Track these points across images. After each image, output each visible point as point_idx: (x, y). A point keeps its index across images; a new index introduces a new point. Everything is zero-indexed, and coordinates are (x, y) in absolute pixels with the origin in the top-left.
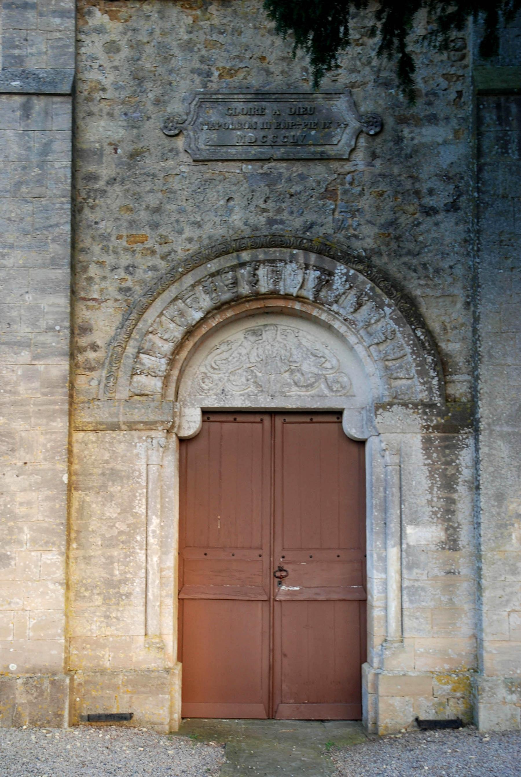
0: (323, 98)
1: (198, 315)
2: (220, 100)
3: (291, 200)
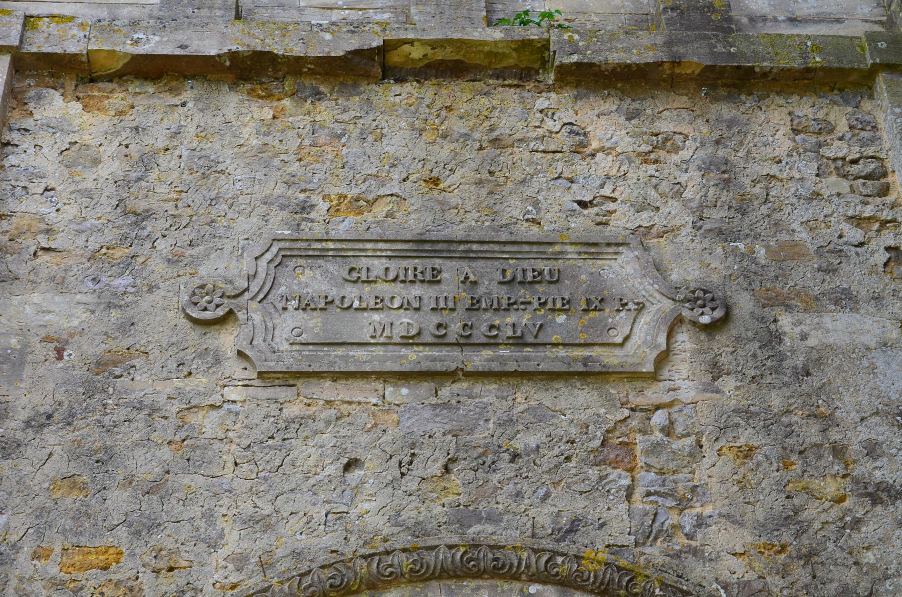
0: (580, 253)
2: (331, 253)
3: (516, 466)
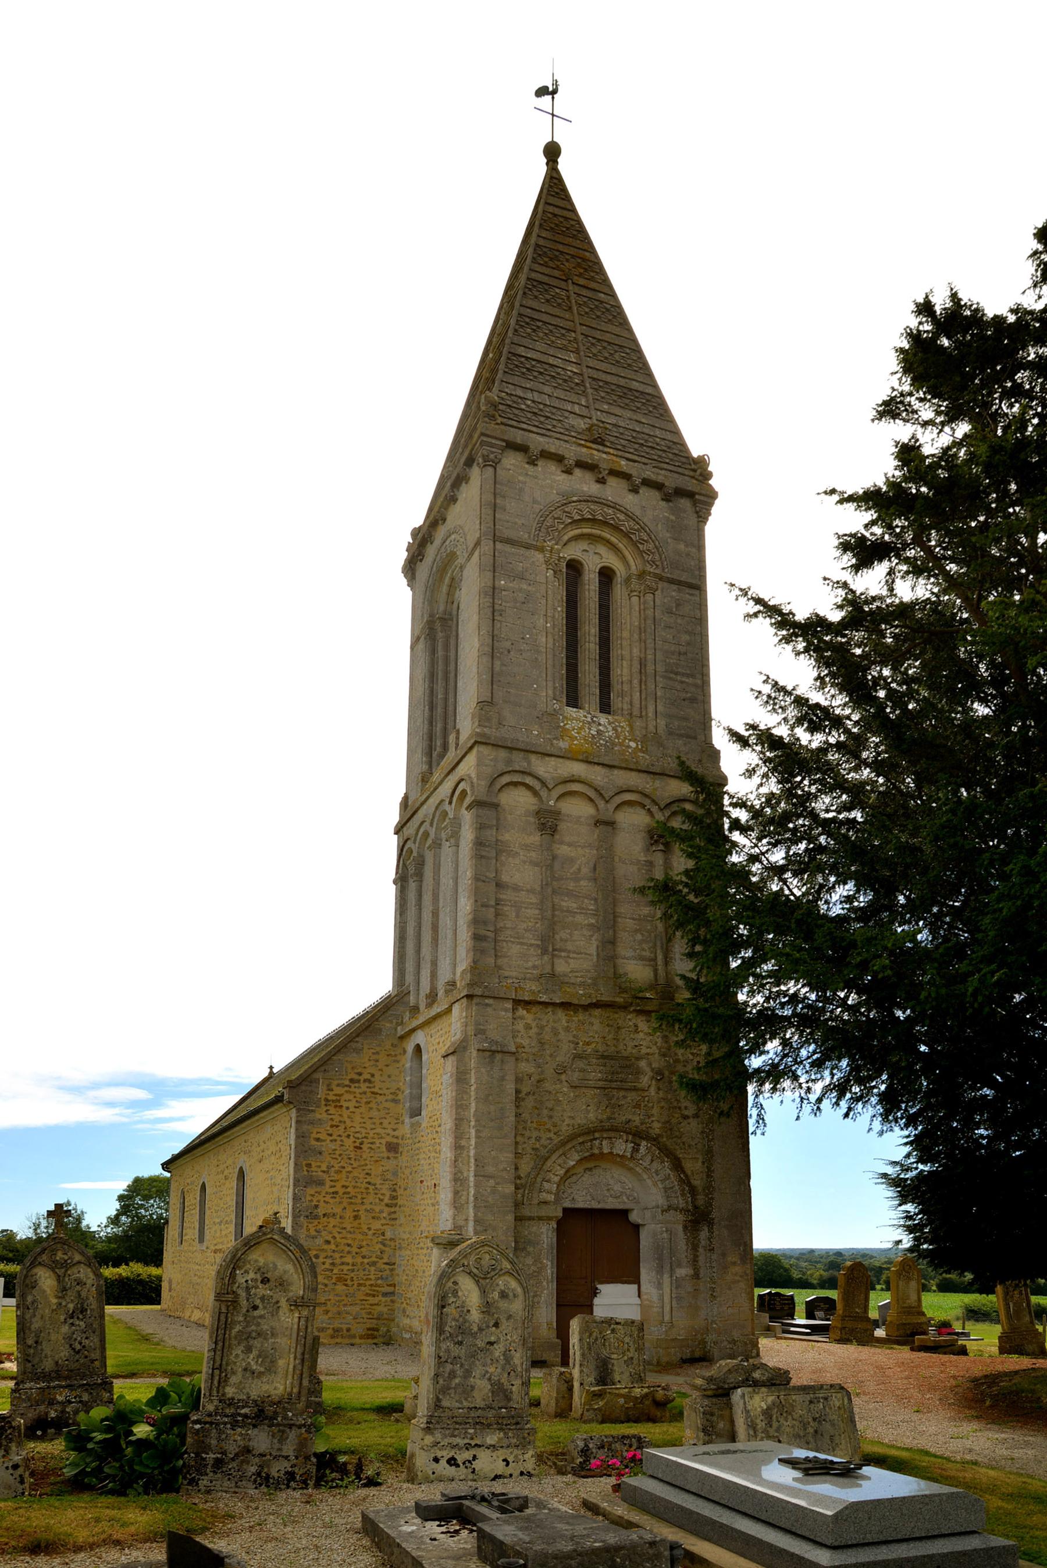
1: (572, 1163)
